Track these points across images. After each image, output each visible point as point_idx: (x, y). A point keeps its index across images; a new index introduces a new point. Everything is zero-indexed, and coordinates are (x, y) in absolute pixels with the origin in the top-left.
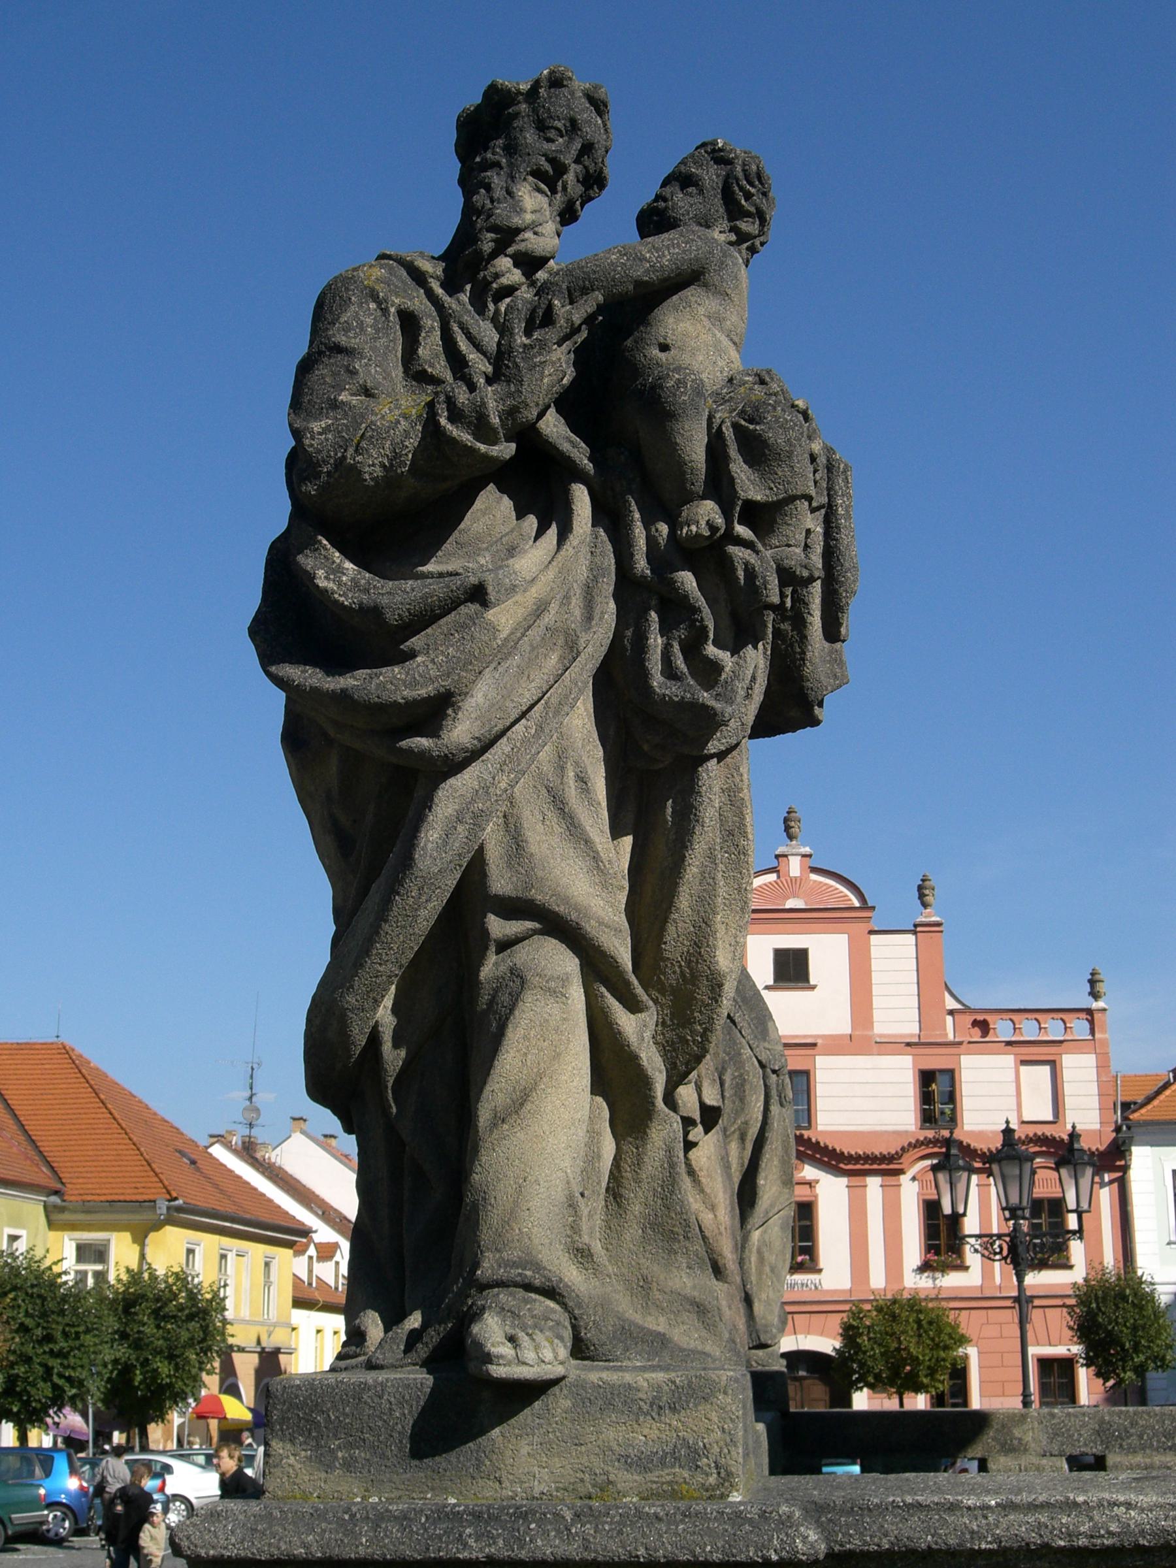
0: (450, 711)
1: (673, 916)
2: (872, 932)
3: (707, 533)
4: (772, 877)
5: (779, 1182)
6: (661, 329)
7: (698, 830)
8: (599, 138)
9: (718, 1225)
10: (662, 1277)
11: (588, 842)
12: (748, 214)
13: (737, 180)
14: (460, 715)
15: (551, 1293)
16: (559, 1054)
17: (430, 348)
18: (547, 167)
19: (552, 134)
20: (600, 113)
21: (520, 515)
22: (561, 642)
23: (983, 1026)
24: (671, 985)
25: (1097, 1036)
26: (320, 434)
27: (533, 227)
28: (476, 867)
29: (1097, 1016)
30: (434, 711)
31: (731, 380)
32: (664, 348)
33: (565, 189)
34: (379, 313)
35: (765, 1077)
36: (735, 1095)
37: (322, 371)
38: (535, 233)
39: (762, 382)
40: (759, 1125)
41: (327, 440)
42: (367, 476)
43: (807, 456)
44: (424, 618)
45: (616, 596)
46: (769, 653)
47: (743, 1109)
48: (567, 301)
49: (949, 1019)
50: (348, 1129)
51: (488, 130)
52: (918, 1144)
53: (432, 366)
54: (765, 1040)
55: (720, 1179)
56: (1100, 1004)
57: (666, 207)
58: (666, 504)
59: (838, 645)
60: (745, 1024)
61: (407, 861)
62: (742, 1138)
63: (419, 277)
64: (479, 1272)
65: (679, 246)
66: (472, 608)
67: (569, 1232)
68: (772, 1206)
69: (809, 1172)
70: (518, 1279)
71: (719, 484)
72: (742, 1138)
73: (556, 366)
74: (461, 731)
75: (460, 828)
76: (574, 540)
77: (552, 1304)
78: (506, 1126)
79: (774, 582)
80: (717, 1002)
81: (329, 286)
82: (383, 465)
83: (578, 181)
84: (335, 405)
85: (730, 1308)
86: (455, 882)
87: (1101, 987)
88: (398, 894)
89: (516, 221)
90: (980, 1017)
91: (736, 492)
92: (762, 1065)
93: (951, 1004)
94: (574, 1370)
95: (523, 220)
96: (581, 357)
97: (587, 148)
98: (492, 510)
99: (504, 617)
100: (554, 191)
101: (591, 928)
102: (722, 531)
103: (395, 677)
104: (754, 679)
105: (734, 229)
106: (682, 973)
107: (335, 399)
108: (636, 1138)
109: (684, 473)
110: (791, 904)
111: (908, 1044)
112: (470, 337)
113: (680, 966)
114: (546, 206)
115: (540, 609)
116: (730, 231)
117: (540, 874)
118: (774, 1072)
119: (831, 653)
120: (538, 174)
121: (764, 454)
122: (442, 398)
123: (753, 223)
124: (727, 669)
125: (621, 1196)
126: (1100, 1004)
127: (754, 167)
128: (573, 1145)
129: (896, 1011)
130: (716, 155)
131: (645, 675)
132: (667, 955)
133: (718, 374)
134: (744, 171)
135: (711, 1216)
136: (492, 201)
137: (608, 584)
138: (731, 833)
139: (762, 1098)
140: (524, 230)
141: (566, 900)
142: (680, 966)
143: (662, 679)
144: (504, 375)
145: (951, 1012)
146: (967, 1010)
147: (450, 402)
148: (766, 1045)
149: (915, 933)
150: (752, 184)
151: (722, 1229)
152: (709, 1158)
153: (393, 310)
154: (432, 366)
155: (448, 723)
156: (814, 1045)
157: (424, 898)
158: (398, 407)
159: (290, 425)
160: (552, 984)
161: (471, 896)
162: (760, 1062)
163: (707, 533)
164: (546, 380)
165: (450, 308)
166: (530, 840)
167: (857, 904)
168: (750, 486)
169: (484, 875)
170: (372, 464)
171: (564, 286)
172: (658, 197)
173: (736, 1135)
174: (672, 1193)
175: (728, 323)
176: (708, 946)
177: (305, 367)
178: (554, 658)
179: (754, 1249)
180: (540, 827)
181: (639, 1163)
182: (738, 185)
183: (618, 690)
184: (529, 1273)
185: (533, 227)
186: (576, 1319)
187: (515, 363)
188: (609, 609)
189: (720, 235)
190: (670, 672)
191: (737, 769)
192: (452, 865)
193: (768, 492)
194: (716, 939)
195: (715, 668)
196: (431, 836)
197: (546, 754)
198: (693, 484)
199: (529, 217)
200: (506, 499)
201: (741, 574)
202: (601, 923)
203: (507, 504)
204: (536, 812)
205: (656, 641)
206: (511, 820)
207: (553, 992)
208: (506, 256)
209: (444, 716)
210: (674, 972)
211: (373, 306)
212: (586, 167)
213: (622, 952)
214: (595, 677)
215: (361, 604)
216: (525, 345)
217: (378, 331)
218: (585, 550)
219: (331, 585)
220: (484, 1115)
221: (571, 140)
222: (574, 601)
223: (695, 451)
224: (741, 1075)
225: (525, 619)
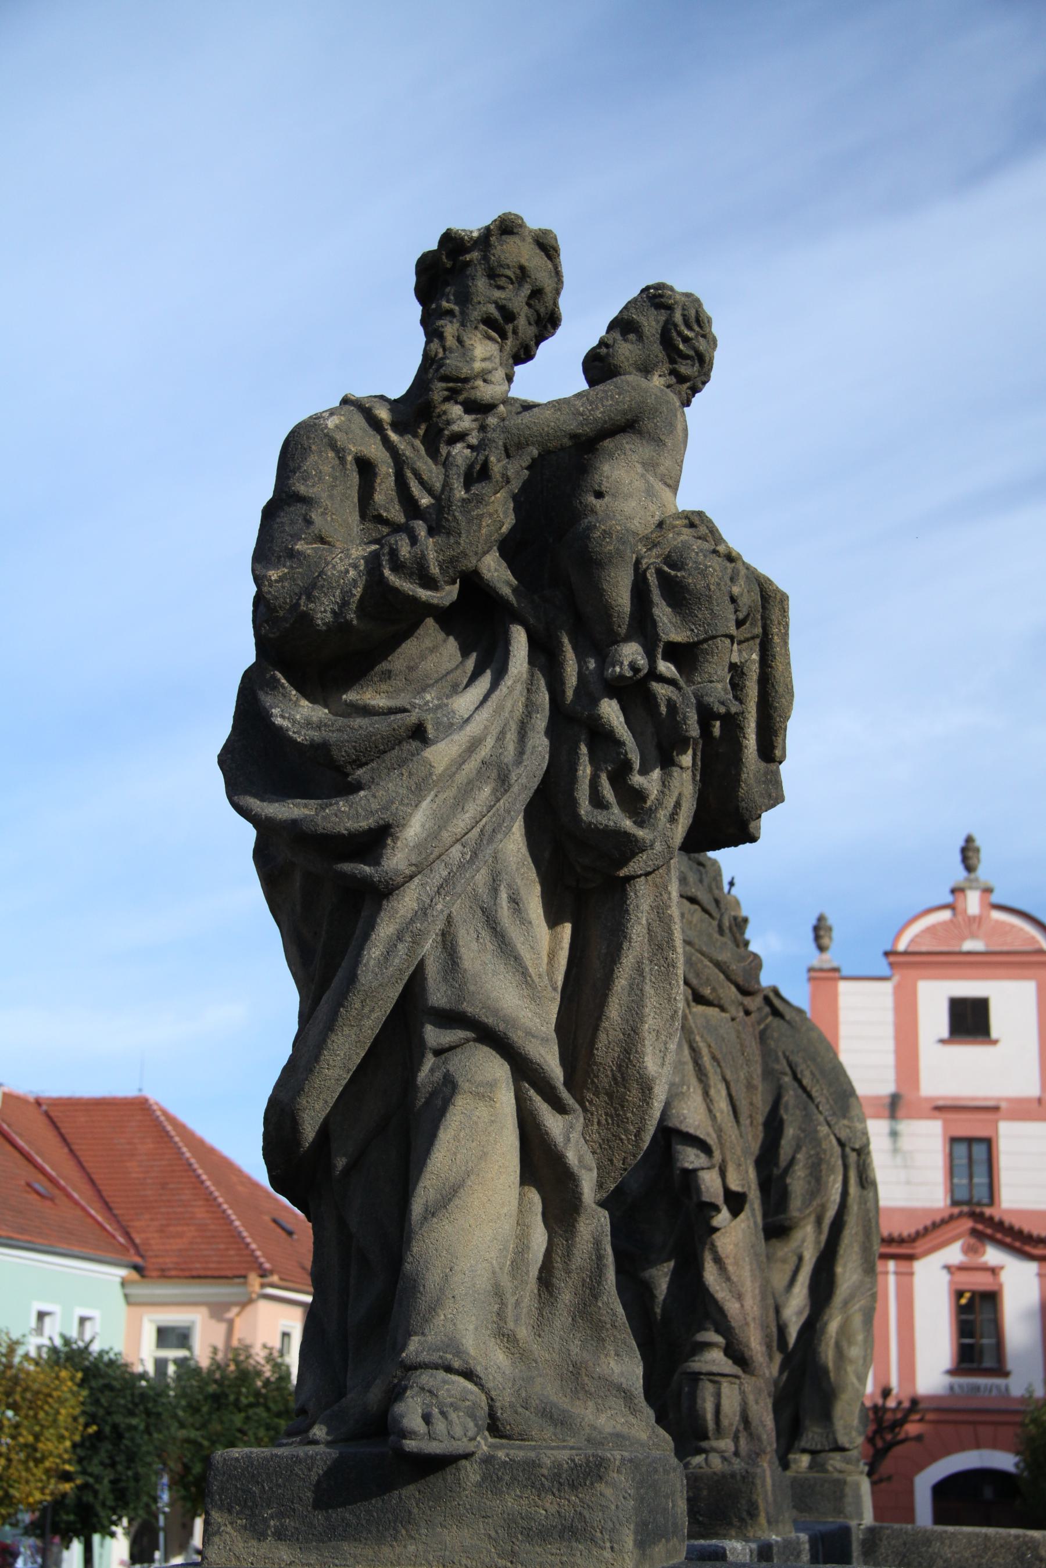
0: (389, 841)
1: (603, 1025)
3: (629, 674)
4: (946, 915)
5: (859, 1270)
6: (596, 476)
7: (625, 946)
8: (547, 283)
9: (745, 1315)
10: (590, 1364)
11: (517, 959)
12: (686, 357)
13: (676, 326)
14: (399, 844)
15: (469, 1375)
16: (485, 1154)
17: (385, 492)
18: (496, 314)
19: (502, 282)
20: (550, 257)
21: (465, 653)
22: (494, 775)
24: (604, 1088)
26: (276, 581)
27: (485, 376)
28: (416, 983)
30: (375, 840)
31: (660, 525)
32: (599, 495)
33: (515, 332)
34: (337, 462)
36: (811, 1174)
37: (283, 518)
38: (485, 381)
39: (692, 525)
40: (836, 1207)
41: (283, 587)
42: (319, 622)
43: (727, 598)
44: (375, 751)
45: (550, 732)
46: (698, 778)
47: (818, 1191)
48: (503, 456)
50: (309, 1221)
51: (448, 274)
53: (387, 510)
54: (844, 1117)
55: (748, 1268)
57: (608, 354)
58: (598, 642)
59: (772, 766)
60: (824, 1100)
61: (352, 979)
62: (819, 1221)
63: (375, 424)
64: (404, 1355)
65: (612, 398)
66: (415, 744)
67: (495, 1319)
69: (993, 1256)
70: (440, 1361)
71: (643, 626)
72: (819, 1221)
73: (498, 512)
74: (397, 859)
75: (400, 946)
76: (508, 681)
77: (470, 1386)
78: (435, 1220)
79: (693, 717)
80: (648, 1104)
81: (292, 433)
82: (333, 611)
83: (530, 324)
84: (292, 554)
85: (757, 1403)
86: (397, 994)
88: (343, 1007)
89: (465, 371)
91: (658, 635)
92: (841, 1144)
94: (484, 1444)
95: (472, 369)
96: (522, 502)
97: (537, 293)
98: (435, 651)
99: (441, 754)
100: (503, 336)
101: (517, 1037)
102: (646, 671)
103: (339, 810)
104: (678, 805)
105: (673, 372)
106: (615, 1079)
107: (292, 549)
108: (566, 1231)
109: (610, 616)
110: (969, 945)
112: (422, 482)
113: (612, 1070)
114: (496, 353)
115: (474, 745)
116: (670, 374)
117: (472, 988)
118: (854, 1150)
119: (766, 773)
120: (488, 321)
121: (685, 598)
122: (386, 550)
123: (693, 366)
124: (652, 797)
125: (553, 1285)
127: (693, 313)
128: (499, 1238)
130: (657, 300)
131: (574, 803)
132: (599, 1060)
133: (650, 518)
134: (684, 315)
135: (737, 1305)
136: (444, 350)
137: (541, 721)
138: (660, 947)
139: (840, 1178)
140: (475, 378)
141: (496, 1012)
142: (612, 1070)
143: (589, 808)
144: (444, 527)
147: (394, 553)
148: (846, 1122)
150: (690, 328)
151: (749, 1319)
152: (736, 1245)
153: (350, 458)
154: (387, 510)
155: (388, 851)
156: (996, 1109)
157: (366, 1010)
158: (348, 556)
159: (253, 571)
160: (481, 1090)
161: (411, 1008)
162: (839, 1141)
163: (629, 674)
164: (484, 531)
165: (404, 455)
166: (465, 957)
168: (671, 627)
169: (423, 989)
170: (323, 611)
171: (501, 443)
172: (602, 343)
174: (599, 1283)
175: (662, 468)
176: (637, 1052)
177: (270, 512)
178: (487, 790)
179: (832, 1342)
180: (474, 946)
181: (568, 1255)
182: (676, 330)
183: (549, 818)
184: (449, 1356)
185: (485, 376)
186: (492, 1399)
187: (455, 517)
188: (540, 743)
189: (657, 381)
190: (598, 801)
191: (666, 888)
192: (394, 980)
193: (689, 633)
194: (644, 1046)
195: (640, 795)
196: (374, 952)
197: (481, 877)
198: (620, 626)
199: (478, 365)
200: (451, 639)
201: (663, 709)
202: (529, 1033)
203: (452, 645)
204: (471, 931)
205: (585, 770)
206: (449, 938)
207: (481, 1096)
208: (456, 403)
209: (384, 846)
210: (607, 1076)
211: (331, 454)
212: (537, 311)
213: (549, 1058)
214: (526, 810)
215: (312, 740)
216: (463, 500)
217: (335, 478)
218: (519, 688)
219: (285, 723)
220: (417, 1208)
221: (520, 285)
222: (508, 736)
223: (622, 598)
224: (818, 1154)
225: (460, 756)
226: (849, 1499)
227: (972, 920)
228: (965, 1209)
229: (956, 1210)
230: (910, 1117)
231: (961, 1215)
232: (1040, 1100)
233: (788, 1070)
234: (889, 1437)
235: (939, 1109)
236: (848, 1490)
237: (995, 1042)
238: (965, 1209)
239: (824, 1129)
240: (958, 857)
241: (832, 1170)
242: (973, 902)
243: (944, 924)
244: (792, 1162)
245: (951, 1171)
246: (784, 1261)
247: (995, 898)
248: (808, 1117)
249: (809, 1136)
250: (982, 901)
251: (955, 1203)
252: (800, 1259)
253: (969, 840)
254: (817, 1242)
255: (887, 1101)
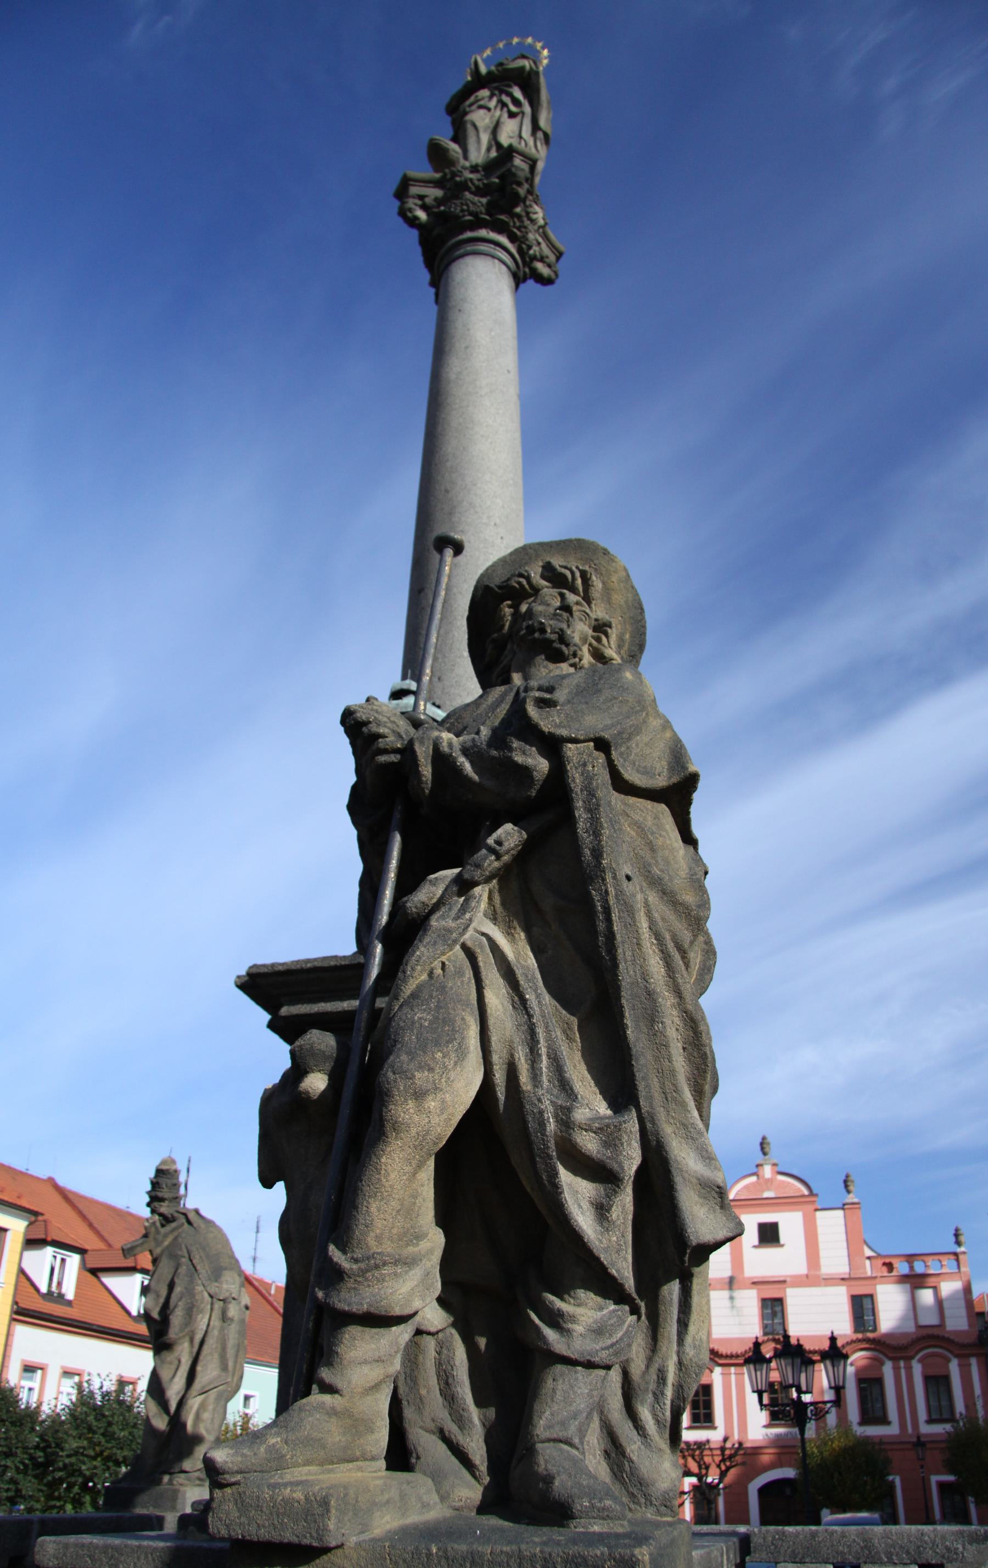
2: (816, 1210)
4: (754, 1179)
23: (890, 1267)
25: (963, 1269)
29: (961, 1257)
35: (212, 1304)
49: (868, 1262)
52: (853, 1342)
54: (216, 1281)
56: (962, 1249)
62: (192, 1340)
68: (209, 1384)
72: (192, 1340)
87: (962, 1238)
90: (887, 1260)
92: (211, 1297)
93: (868, 1253)
111: (843, 1279)
126: (962, 1249)
129: (835, 1259)
139: (208, 1316)
145: (869, 1258)
146: (879, 1256)
148: (216, 1284)
149: (843, 1209)
156: (784, 1282)
167: (806, 1192)
173: (187, 1339)
226: (180, 1501)
227: (768, 1180)
228: (771, 1337)
229: (766, 1338)
230: (740, 1289)
231: (768, 1340)
232: (807, 1276)
233: (187, 1255)
234: (728, 1464)
235: (754, 1283)
236: (180, 1496)
237: (782, 1246)
238: (771, 1337)
239: (200, 1288)
240: (759, 1148)
241: (202, 1311)
242: (767, 1171)
243: (753, 1184)
244: (176, 1306)
245: (763, 1317)
246: (171, 1363)
247: (779, 1169)
248: (192, 1281)
249: (190, 1292)
250: (772, 1170)
251: (765, 1334)
252: (180, 1361)
253: (764, 1138)
254: (191, 1352)
255: (727, 1280)
